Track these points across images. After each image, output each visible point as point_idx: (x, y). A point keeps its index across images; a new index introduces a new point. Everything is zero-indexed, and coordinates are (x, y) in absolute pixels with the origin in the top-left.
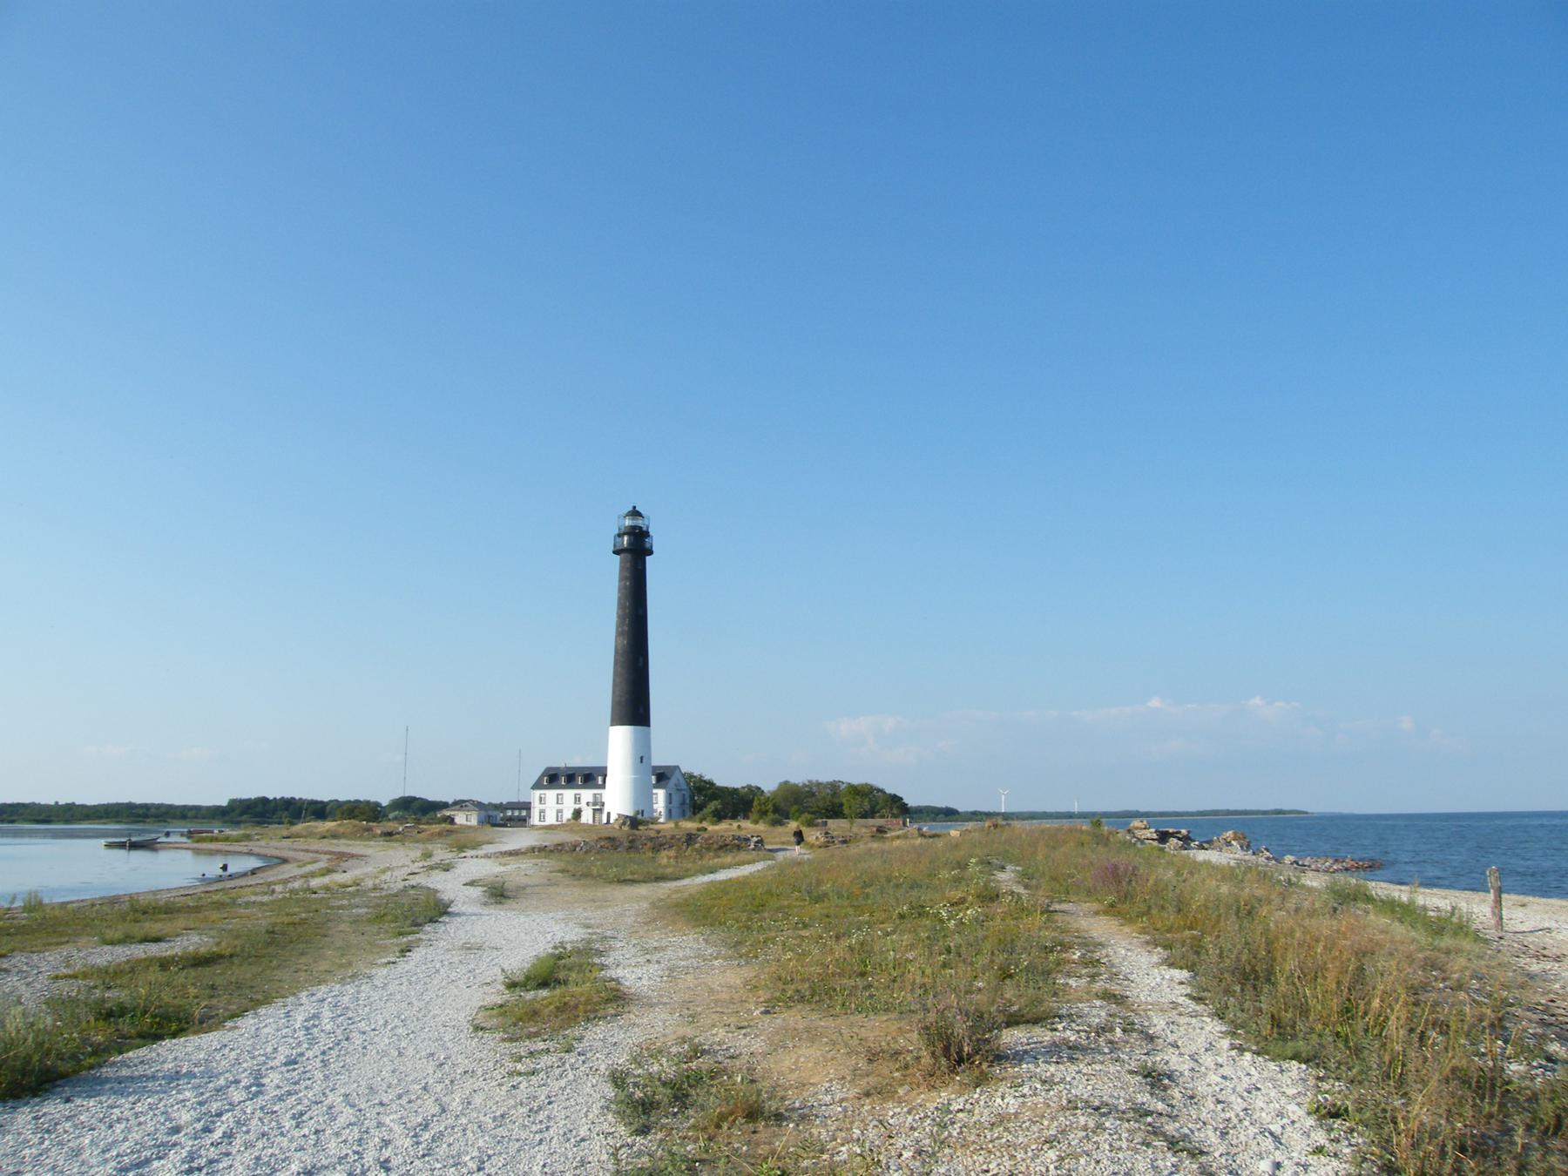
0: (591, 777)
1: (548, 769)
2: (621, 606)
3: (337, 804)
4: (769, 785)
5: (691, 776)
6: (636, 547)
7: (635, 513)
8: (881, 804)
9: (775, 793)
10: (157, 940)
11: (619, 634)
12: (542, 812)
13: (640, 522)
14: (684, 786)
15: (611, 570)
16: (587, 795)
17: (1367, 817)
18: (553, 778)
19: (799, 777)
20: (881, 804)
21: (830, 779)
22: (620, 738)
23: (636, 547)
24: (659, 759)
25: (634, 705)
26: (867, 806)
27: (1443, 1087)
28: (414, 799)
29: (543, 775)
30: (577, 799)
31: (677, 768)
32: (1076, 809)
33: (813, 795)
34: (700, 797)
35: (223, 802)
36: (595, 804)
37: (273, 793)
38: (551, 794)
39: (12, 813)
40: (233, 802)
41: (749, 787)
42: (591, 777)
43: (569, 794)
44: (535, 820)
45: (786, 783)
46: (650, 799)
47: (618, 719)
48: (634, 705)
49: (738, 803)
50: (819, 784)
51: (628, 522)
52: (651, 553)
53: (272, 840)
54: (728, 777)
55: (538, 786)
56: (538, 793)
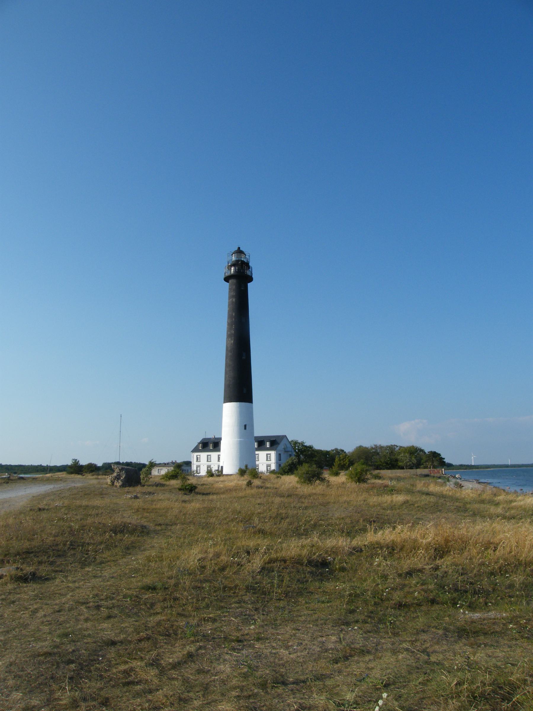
1: (204, 439)
2: (230, 317)
4: (349, 448)
5: (296, 443)
6: (241, 277)
7: (239, 252)
8: (424, 459)
9: (353, 453)
11: (229, 336)
14: (290, 449)
15: (223, 293)
17: (16, 466)
19: (368, 443)
20: (424, 459)
21: (389, 444)
22: (230, 411)
23: (241, 277)
25: (240, 388)
26: (414, 460)
29: (199, 443)
31: (285, 437)
32: (509, 463)
33: (378, 454)
38: (203, 455)
39: (465, 467)
40: (105, 464)
41: (336, 449)
45: (360, 447)
46: (254, 458)
47: (228, 399)
48: (240, 388)
50: (381, 447)
54: (322, 443)
55: (196, 450)
56: (196, 454)
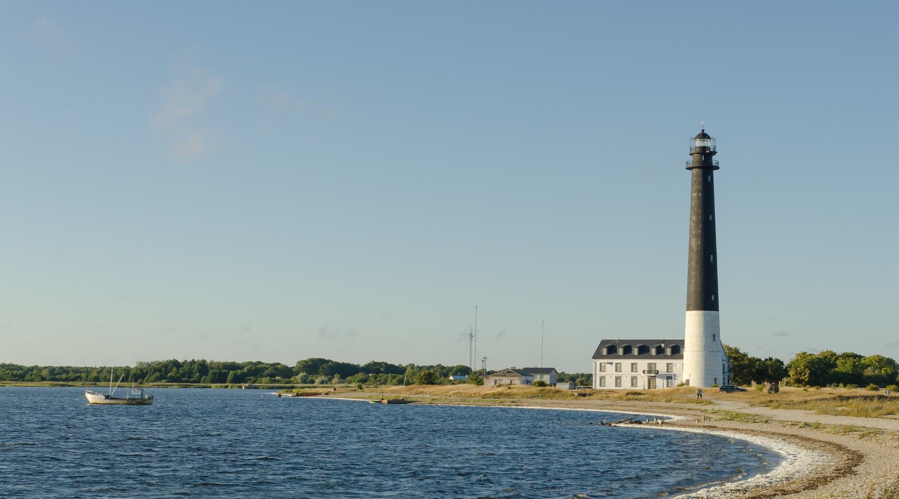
6: (705, 165)
7: (704, 136)
10: (841, 398)
12: (602, 378)
13: (708, 143)
18: (610, 349)
23: (705, 165)
25: (707, 296)
28: (323, 361)
30: (633, 367)
35: (521, 368)
36: (650, 372)
37: (268, 359)
43: (626, 363)
44: (596, 385)
48: (707, 296)
49: (768, 373)
51: (699, 143)
55: (597, 355)
56: (599, 361)
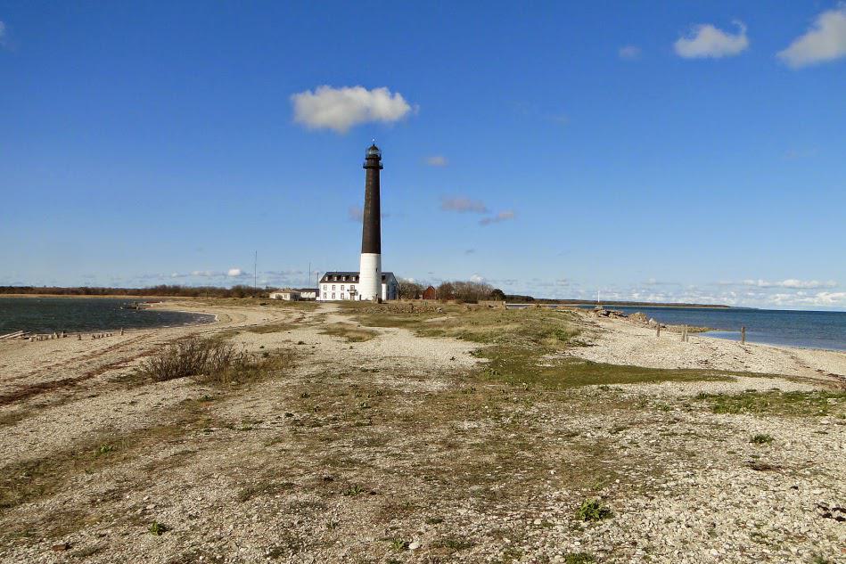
0: (352, 277)
2: (367, 194)
3: (68, 289)
6: (374, 165)
7: (374, 148)
11: (366, 208)
16: (348, 286)
18: (330, 277)
22: (366, 263)
24: (384, 270)
25: (373, 243)
27: (143, 415)
34: (398, 290)
38: (330, 285)
42: (352, 277)
43: (338, 285)
46: (326, 136)
49: (415, 292)
52: (382, 168)
53: (794, 373)
55: (323, 281)
56: (322, 285)
